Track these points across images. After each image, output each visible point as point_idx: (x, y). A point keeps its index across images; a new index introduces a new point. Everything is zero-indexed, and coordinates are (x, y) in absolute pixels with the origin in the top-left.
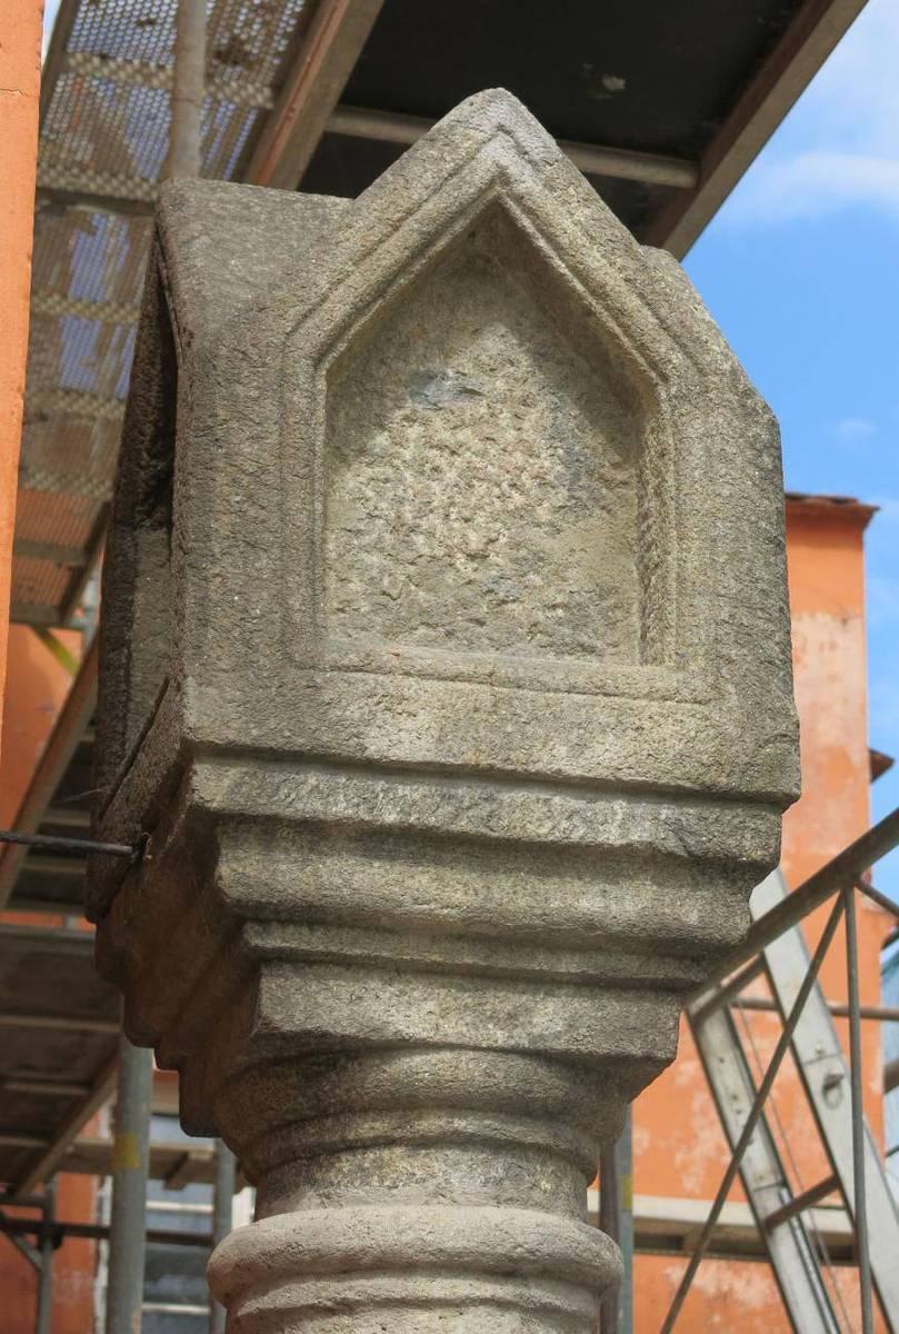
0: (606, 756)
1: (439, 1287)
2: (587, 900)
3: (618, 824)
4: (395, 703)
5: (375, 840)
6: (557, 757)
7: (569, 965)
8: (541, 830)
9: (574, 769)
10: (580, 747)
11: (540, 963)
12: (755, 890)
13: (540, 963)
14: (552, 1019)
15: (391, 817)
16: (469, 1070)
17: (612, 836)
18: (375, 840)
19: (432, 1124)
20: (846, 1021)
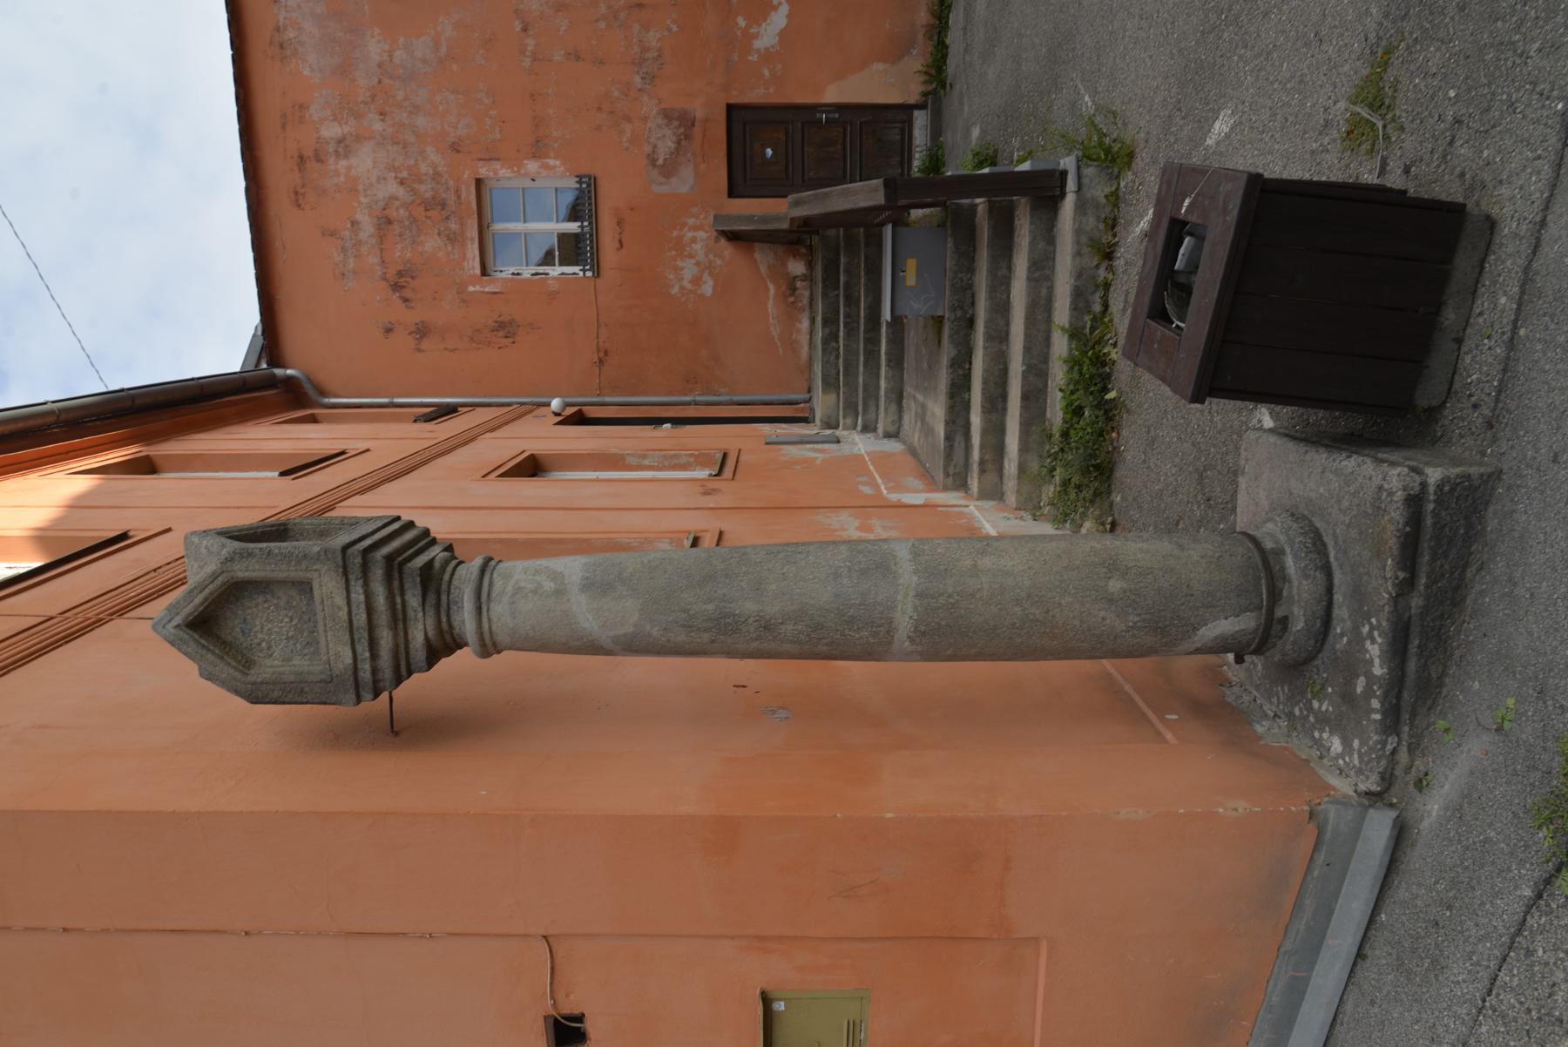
0: (340, 600)
1: (485, 620)
2: (381, 600)
3: (358, 596)
4: (337, 655)
5: (374, 657)
6: (343, 614)
7: (398, 600)
8: (364, 616)
9: (346, 609)
10: (340, 608)
11: (399, 607)
12: (196, 667)
13: (399, 607)
14: (413, 601)
15: (367, 654)
16: (430, 622)
17: (362, 598)
18: (374, 657)
19: (445, 626)
20: (221, 343)
